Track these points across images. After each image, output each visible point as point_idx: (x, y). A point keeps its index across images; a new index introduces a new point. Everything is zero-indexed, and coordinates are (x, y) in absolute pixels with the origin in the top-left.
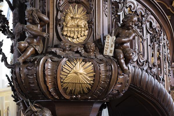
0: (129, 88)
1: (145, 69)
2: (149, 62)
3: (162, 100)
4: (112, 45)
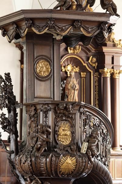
1: (99, 159)
4: (86, 147)
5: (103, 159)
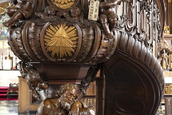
1: (133, 34)
2: (137, 28)
3: (149, 64)
4: (96, 10)
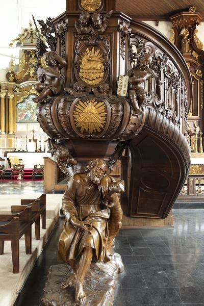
0: (143, 128)
1: (161, 111)
4: (125, 85)
5: (170, 113)
